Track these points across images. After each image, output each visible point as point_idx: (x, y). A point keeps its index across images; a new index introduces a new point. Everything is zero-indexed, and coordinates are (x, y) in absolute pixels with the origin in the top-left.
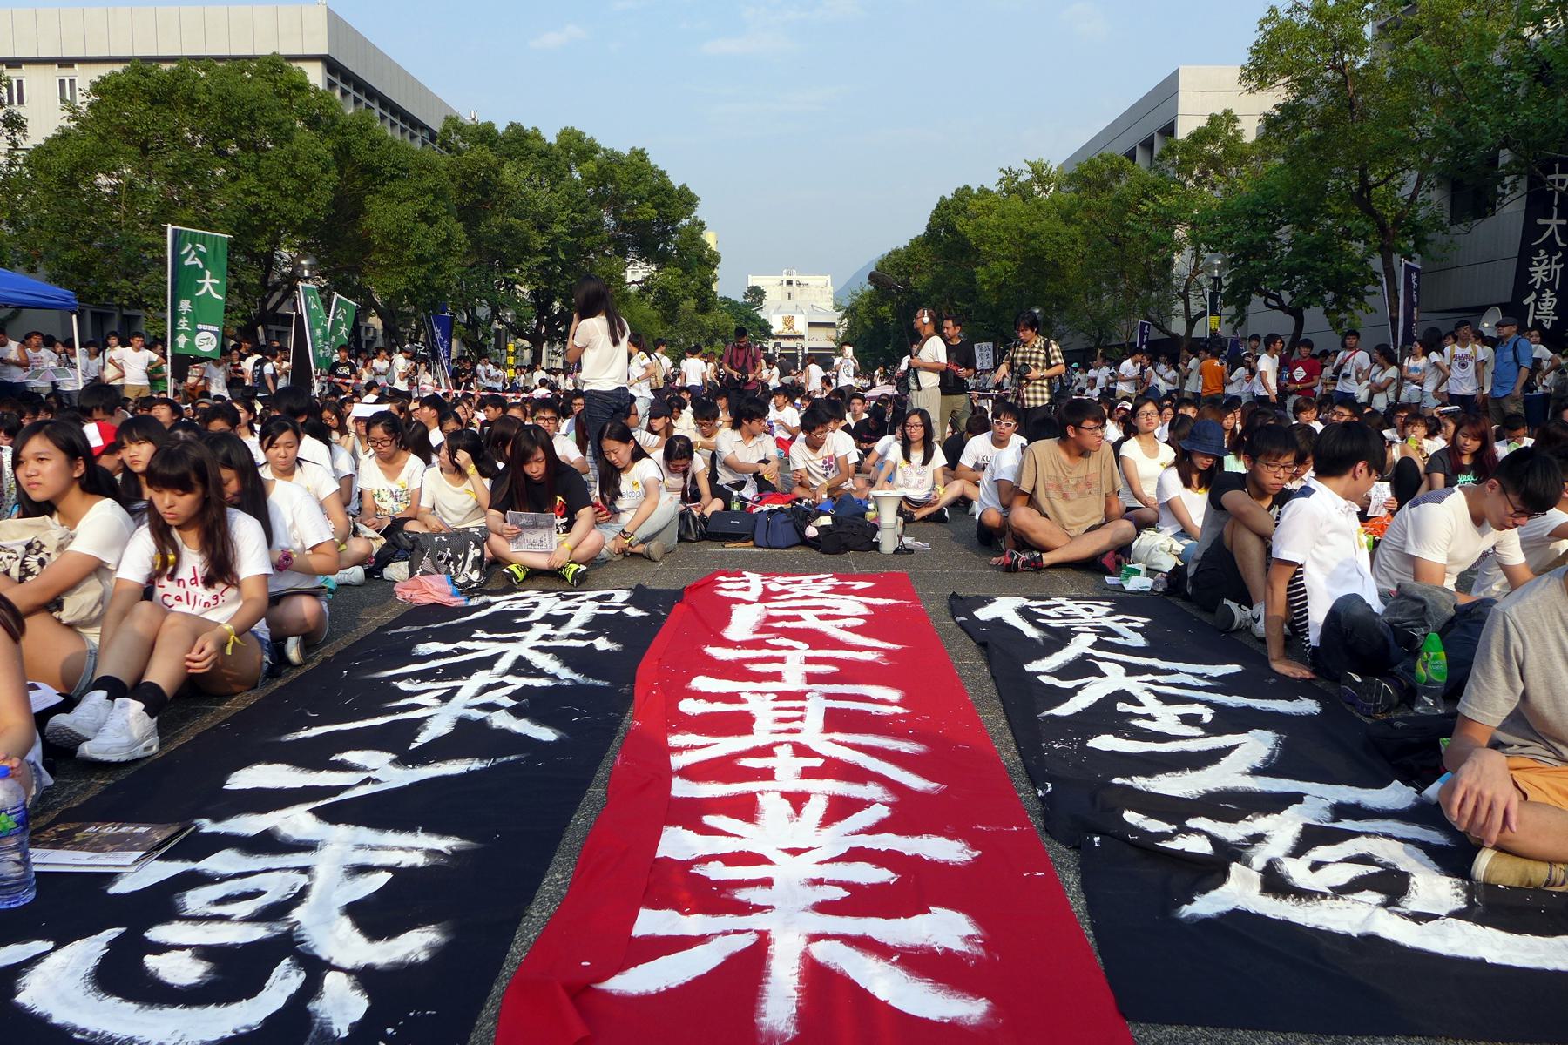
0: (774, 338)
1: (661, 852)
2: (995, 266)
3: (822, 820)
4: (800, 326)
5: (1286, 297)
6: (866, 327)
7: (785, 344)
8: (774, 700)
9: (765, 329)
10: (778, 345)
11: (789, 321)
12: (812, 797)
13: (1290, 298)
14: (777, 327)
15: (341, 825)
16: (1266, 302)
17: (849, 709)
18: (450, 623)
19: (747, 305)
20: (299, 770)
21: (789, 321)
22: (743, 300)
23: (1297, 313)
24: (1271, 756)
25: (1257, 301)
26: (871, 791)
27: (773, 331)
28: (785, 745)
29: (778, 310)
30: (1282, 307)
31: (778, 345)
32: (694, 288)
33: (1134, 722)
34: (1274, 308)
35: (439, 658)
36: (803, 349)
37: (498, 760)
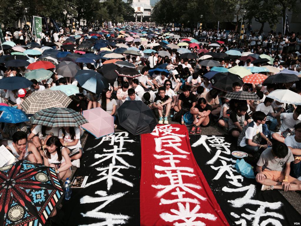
0: (135, 13)
1: (160, 215)
2: (192, 4)
3: (190, 209)
4: (142, 10)
5: (260, 19)
6: (159, 13)
7: (138, 15)
8: (172, 173)
9: (133, 10)
10: (136, 15)
11: (139, 9)
12: (186, 203)
13: (261, 19)
14: (136, 10)
15: (107, 213)
16: (256, 20)
17: (185, 175)
18: (97, 146)
19: (128, 4)
20: (91, 197)
21: (139, 9)
22: (127, 2)
23: (263, 23)
24: (254, 193)
25: (254, 19)
26: (195, 201)
27: (135, 12)
28: (178, 188)
29: (136, 5)
30: (259, 21)
31: (136, 15)
32: (117, 5)
33: (239, 77)
34: (258, 21)
35: (101, 159)
36: (143, 16)
37: (126, 193)
